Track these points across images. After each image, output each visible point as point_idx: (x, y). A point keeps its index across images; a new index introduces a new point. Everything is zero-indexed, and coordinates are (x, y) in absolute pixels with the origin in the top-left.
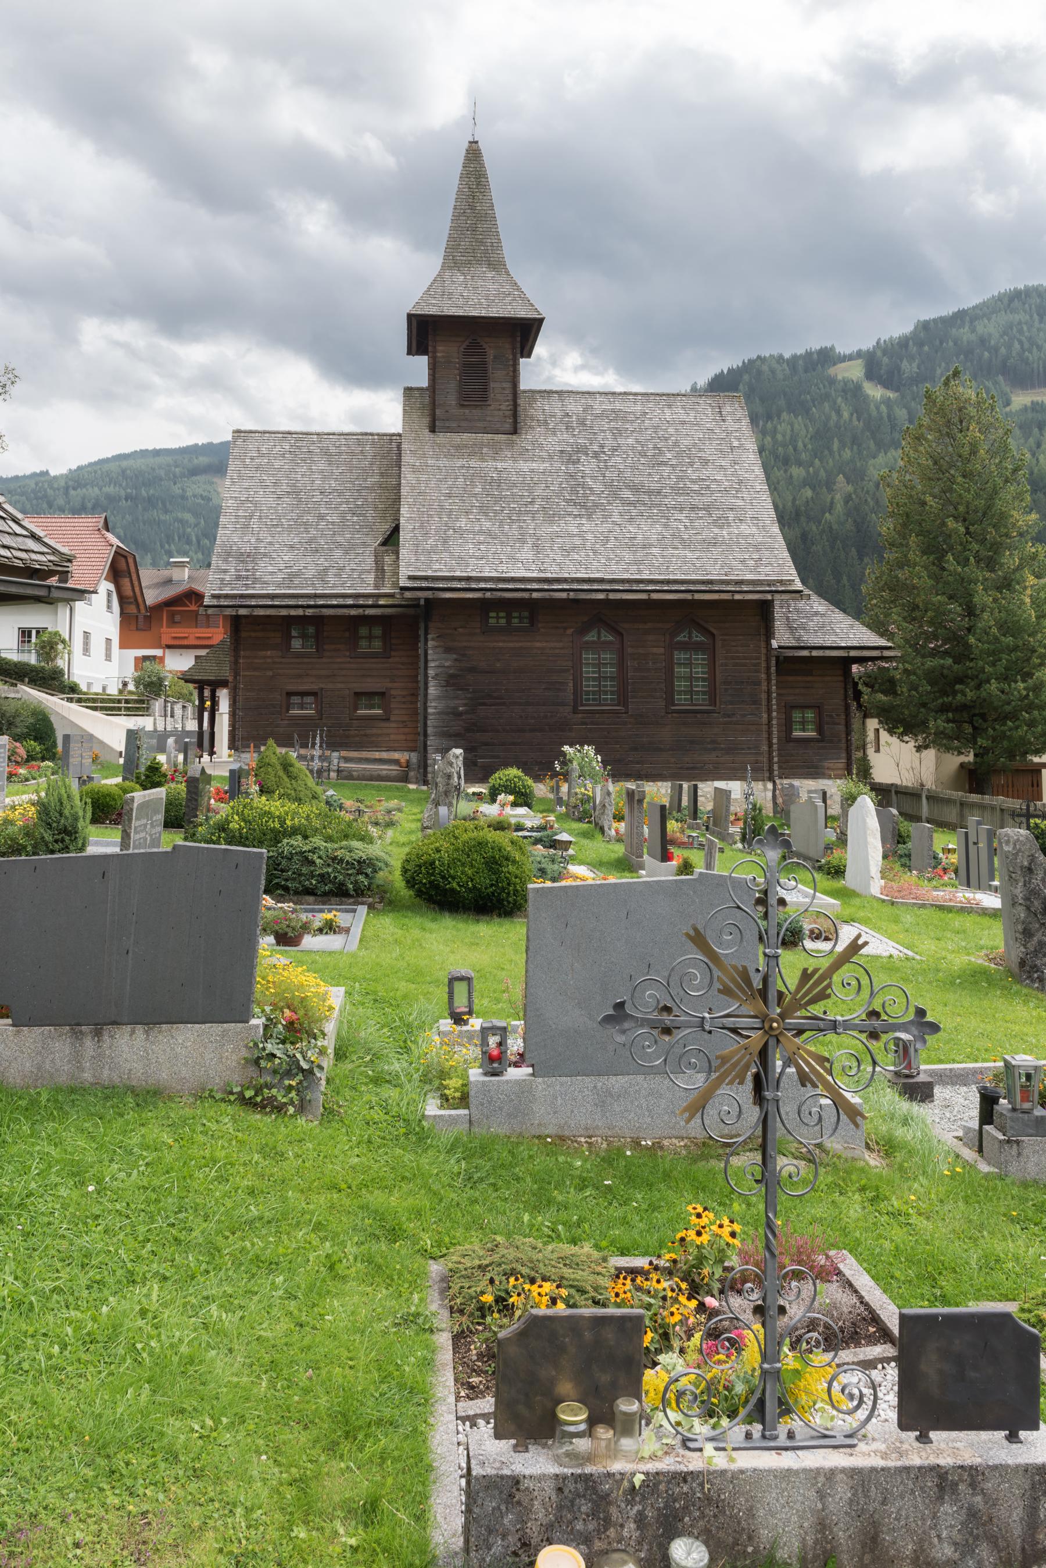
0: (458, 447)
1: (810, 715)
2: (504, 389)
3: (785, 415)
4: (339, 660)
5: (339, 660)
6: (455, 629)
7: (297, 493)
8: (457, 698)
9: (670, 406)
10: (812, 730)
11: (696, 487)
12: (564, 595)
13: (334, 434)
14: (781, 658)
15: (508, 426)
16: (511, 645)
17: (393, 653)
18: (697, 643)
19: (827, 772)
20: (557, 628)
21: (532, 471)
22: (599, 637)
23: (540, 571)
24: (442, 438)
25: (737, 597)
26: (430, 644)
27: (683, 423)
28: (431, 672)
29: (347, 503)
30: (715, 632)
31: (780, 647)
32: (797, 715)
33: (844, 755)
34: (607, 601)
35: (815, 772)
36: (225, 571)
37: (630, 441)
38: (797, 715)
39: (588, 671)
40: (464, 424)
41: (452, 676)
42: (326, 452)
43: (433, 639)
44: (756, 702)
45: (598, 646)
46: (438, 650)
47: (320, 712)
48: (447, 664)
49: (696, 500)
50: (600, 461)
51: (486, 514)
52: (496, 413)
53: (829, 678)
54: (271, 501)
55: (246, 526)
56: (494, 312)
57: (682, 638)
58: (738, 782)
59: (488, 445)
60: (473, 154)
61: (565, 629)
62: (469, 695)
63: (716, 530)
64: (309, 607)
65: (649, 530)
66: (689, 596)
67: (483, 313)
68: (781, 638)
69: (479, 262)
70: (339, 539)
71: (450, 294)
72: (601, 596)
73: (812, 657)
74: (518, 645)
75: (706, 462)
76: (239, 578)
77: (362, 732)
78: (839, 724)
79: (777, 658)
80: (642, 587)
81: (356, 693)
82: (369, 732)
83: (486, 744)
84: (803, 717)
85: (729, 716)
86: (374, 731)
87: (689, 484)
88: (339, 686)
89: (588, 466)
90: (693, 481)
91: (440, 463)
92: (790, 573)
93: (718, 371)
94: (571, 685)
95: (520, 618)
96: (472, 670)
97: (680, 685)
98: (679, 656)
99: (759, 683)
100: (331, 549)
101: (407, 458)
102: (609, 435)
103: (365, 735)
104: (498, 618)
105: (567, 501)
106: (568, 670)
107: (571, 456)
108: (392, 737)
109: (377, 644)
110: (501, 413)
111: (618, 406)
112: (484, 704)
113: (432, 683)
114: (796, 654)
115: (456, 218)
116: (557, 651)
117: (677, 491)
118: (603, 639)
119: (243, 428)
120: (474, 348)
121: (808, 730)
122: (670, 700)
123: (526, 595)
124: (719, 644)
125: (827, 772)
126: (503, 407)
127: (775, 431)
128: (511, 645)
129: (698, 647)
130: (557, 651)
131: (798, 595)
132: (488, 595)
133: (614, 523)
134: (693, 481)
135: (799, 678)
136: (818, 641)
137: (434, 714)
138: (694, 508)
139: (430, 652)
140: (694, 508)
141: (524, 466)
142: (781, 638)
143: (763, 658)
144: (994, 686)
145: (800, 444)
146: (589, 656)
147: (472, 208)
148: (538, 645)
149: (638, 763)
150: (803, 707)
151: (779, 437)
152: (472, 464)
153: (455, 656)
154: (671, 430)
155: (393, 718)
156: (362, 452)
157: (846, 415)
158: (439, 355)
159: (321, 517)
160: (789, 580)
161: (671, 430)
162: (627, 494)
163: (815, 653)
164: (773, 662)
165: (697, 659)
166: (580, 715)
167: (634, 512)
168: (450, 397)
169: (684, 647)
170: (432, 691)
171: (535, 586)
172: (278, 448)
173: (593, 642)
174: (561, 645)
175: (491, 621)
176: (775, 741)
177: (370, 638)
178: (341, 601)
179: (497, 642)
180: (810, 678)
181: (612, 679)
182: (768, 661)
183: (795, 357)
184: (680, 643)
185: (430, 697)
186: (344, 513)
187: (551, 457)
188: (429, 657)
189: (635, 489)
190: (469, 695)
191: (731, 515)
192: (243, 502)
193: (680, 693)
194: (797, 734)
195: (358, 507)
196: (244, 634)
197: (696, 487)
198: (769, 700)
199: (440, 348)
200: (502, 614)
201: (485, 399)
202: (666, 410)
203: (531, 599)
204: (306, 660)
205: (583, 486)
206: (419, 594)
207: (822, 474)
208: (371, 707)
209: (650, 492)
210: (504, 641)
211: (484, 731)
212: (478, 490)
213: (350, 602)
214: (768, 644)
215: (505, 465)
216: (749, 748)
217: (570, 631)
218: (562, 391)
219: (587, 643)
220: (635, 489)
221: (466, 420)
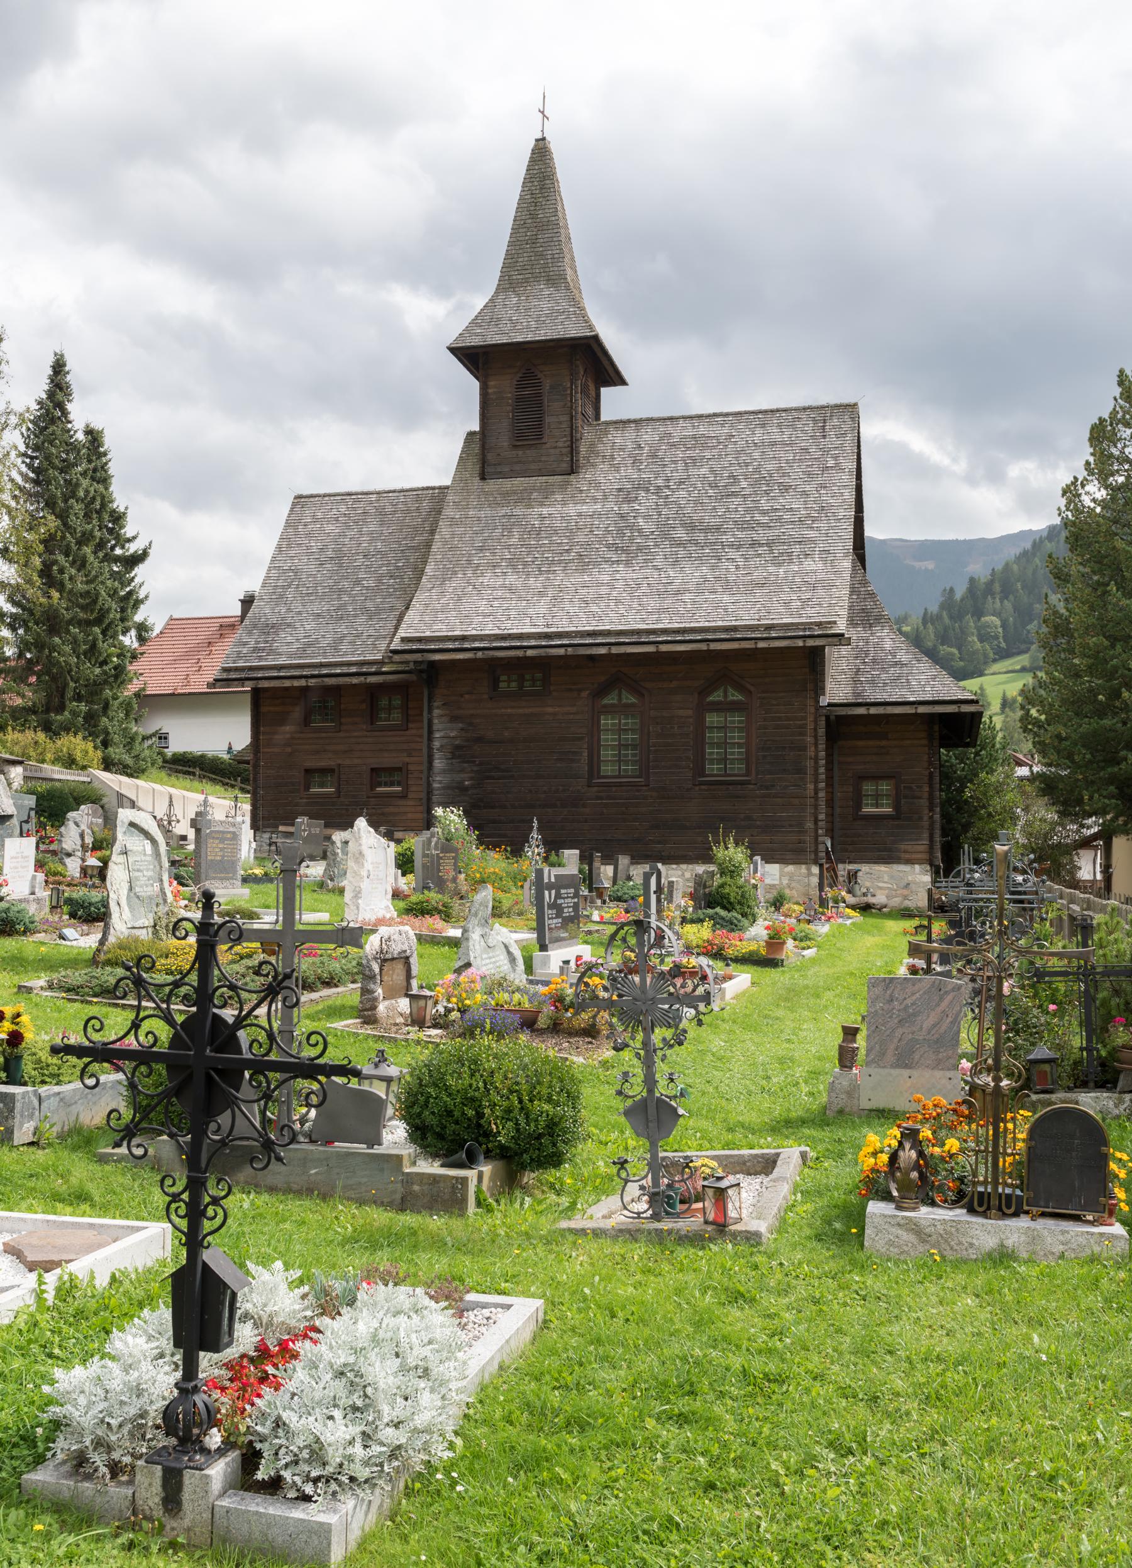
0: (505, 495)
1: (885, 787)
2: (560, 423)
4: (356, 734)
5: (356, 734)
6: (462, 696)
7: (340, 558)
8: (462, 771)
9: (763, 426)
10: (888, 805)
11: (765, 519)
12: (562, 651)
13: (394, 491)
14: (832, 718)
15: (565, 466)
16: (521, 711)
17: (410, 725)
18: (733, 703)
19: (903, 855)
20: (571, 690)
21: (580, 515)
22: (620, 699)
23: (548, 626)
24: (492, 485)
26: (436, 712)
27: (773, 444)
28: (436, 744)
29: (388, 565)
30: (752, 689)
31: (830, 705)
32: (868, 787)
33: (926, 835)
34: (609, 656)
35: (887, 856)
36: (245, 644)
37: (703, 471)
40: (517, 467)
41: (458, 747)
42: (381, 512)
43: (438, 708)
44: (801, 771)
46: (443, 719)
47: (338, 791)
48: (452, 735)
50: (660, 497)
51: (514, 567)
52: (552, 451)
53: (908, 742)
54: (313, 568)
56: (542, 334)
57: (716, 696)
58: (777, 866)
59: (539, 490)
60: (541, 154)
61: (580, 690)
62: (475, 768)
63: (771, 569)
64: (313, 676)
65: (692, 573)
67: (530, 337)
68: (837, 689)
69: (537, 279)
71: (499, 319)
72: (603, 651)
73: (869, 715)
74: (527, 711)
75: (786, 488)
77: (379, 811)
78: (920, 798)
79: (828, 718)
80: (652, 638)
81: (372, 769)
82: (387, 810)
83: (494, 822)
84: (877, 790)
85: (767, 788)
86: (391, 809)
87: (758, 517)
88: (356, 761)
89: (646, 502)
90: (764, 513)
91: (482, 514)
94: (586, 754)
95: (533, 680)
96: (479, 740)
97: (712, 752)
98: (712, 719)
100: (355, 616)
101: (449, 512)
102: (680, 466)
103: (383, 814)
104: (509, 681)
105: (608, 546)
106: (580, 739)
107: (627, 496)
108: (410, 816)
110: (557, 451)
111: (702, 430)
112: (493, 778)
113: (437, 755)
114: (850, 713)
115: (515, 230)
116: (571, 717)
117: (742, 526)
118: (624, 701)
119: (305, 493)
120: (528, 379)
121: (882, 806)
122: (700, 770)
123: (520, 653)
125: (903, 855)
126: (560, 444)
128: (521, 711)
130: (571, 717)
131: (836, 640)
132: (480, 654)
133: (656, 568)
134: (764, 513)
135: (871, 743)
136: (896, 695)
137: (439, 789)
138: (754, 544)
139: (436, 721)
140: (754, 544)
141: (572, 510)
142: (837, 689)
143: (811, 718)
146: (606, 721)
147: (533, 216)
148: (550, 710)
149: (659, 843)
150: (876, 778)
153: (460, 725)
154: (756, 455)
155: (411, 795)
156: (418, 508)
158: (490, 391)
159: (358, 582)
160: (830, 623)
161: (756, 455)
162: (681, 534)
163: (873, 711)
164: (823, 723)
165: (733, 722)
166: (596, 789)
167: (682, 553)
168: (503, 439)
169: (717, 707)
171: (533, 643)
172: (335, 512)
173: (613, 705)
174: (574, 709)
175: (502, 685)
176: (822, 817)
177: (390, 709)
178: (345, 670)
179: (506, 708)
180: (884, 743)
181: (634, 747)
184: (713, 703)
185: (436, 770)
186: (382, 576)
187: (605, 497)
188: (435, 727)
189: (691, 527)
190: (475, 768)
191: (797, 549)
192: (285, 571)
193: (712, 762)
194: (867, 810)
195: (398, 568)
196: (264, 709)
197: (765, 519)
198: (816, 769)
199: (491, 383)
200: (514, 677)
201: (540, 436)
202: (759, 431)
203: (526, 657)
204: (324, 735)
205: (631, 528)
206: (408, 657)
209: (706, 530)
210: (512, 707)
211: (492, 808)
212: (514, 541)
213: (354, 670)
215: (551, 510)
216: (791, 826)
217: (585, 694)
218: (641, 420)
219: (605, 706)
220: (691, 527)
221: (520, 462)
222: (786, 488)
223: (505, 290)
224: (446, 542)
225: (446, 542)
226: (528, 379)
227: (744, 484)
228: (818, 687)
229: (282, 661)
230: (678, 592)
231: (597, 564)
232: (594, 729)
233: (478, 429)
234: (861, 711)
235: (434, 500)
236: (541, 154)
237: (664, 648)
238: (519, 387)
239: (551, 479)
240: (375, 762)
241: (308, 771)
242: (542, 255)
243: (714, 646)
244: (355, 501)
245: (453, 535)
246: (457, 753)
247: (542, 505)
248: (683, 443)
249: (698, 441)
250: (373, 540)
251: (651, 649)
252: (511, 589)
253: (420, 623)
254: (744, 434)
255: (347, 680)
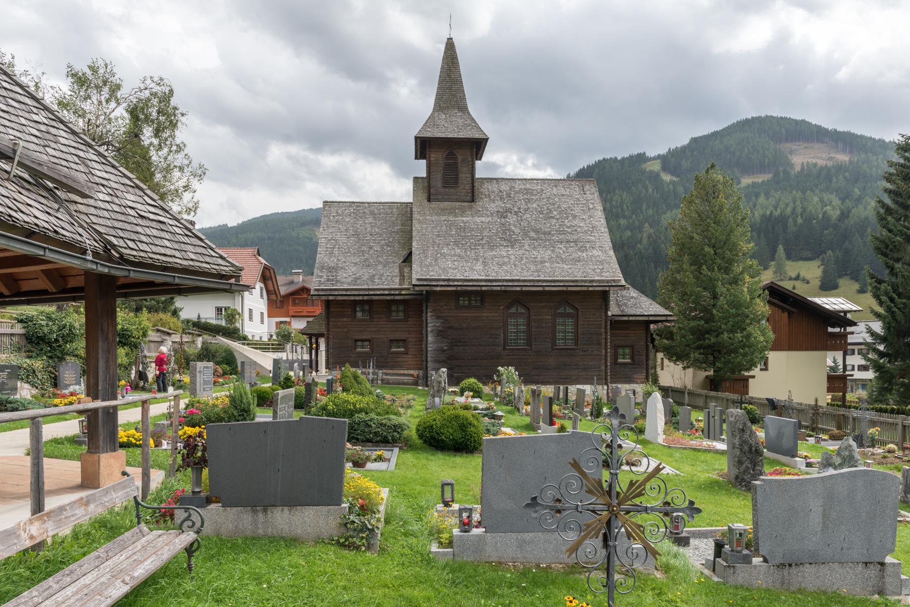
0: (443, 210)
1: (627, 351)
3: (617, 191)
7: (358, 235)
9: (556, 186)
11: (569, 230)
12: (499, 288)
15: (469, 198)
21: (482, 222)
24: (434, 205)
25: (591, 289)
26: (429, 314)
27: (563, 195)
28: (429, 329)
32: (620, 351)
34: (522, 291)
35: (629, 380)
37: (534, 205)
38: (620, 351)
39: (511, 328)
40: (454, 197)
41: (440, 331)
42: (372, 213)
44: (599, 344)
45: (516, 315)
47: (372, 349)
49: (569, 237)
51: (458, 246)
54: (344, 239)
55: (332, 253)
59: (458, 209)
65: (544, 254)
66: (565, 289)
68: (613, 310)
69: (453, 107)
70: (380, 259)
76: (328, 280)
80: (540, 284)
86: (400, 360)
89: (511, 219)
90: (568, 227)
92: (619, 276)
93: (581, 167)
96: (451, 328)
97: (560, 335)
99: (601, 334)
101: (416, 216)
102: (523, 202)
105: (500, 238)
107: (503, 214)
109: (401, 315)
111: (528, 186)
117: (560, 232)
120: (451, 155)
122: (554, 343)
123: (479, 288)
124: (580, 314)
127: (612, 200)
129: (569, 316)
132: (459, 288)
134: (568, 227)
138: (568, 242)
141: (478, 220)
142: (613, 310)
144: (725, 336)
145: (625, 207)
146: (512, 321)
147: (449, 76)
150: (624, 347)
151: (614, 203)
152: (450, 218)
154: (557, 199)
157: (650, 190)
159: (371, 248)
161: (557, 199)
162: (532, 234)
163: (631, 318)
167: (536, 244)
168: (438, 182)
169: (562, 315)
170: (430, 339)
171: (484, 284)
177: (397, 311)
178: (382, 292)
181: (524, 332)
182: (606, 322)
183: (623, 159)
189: (537, 231)
191: (588, 245)
192: (329, 240)
194: (620, 360)
196: (332, 310)
197: (569, 230)
198: (606, 343)
201: (457, 183)
202: (554, 189)
205: (509, 230)
207: (637, 223)
208: (399, 347)
209: (544, 233)
212: (453, 233)
213: (387, 292)
214: (606, 313)
215: (467, 219)
217: (502, 307)
220: (537, 231)
222: (575, 217)
223: (438, 111)
224: (419, 232)
225: (419, 232)
226: (451, 155)
227: (555, 213)
228: (607, 308)
229: (346, 287)
230: (541, 262)
231: (497, 247)
232: (505, 325)
233: (425, 175)
234: (626, 318)
235: (405, 212)
236: (450, 45)
237: (547, 289)
238: (447, 158)
239: (464, 204)
240: (392, 337)
241: (356, 341)
242: (455, 96)
243: (569, 289)
244: (357, 206)
245: (422, 228)
246: (440, 334)
247: (462, 216)
248: (520, 191)
249: (528, 191)
250: (372, 227)
251: (541, 289)
252: (459, 256)
253: (419, 272)
254: (549, 191)
255: (384, 297)
